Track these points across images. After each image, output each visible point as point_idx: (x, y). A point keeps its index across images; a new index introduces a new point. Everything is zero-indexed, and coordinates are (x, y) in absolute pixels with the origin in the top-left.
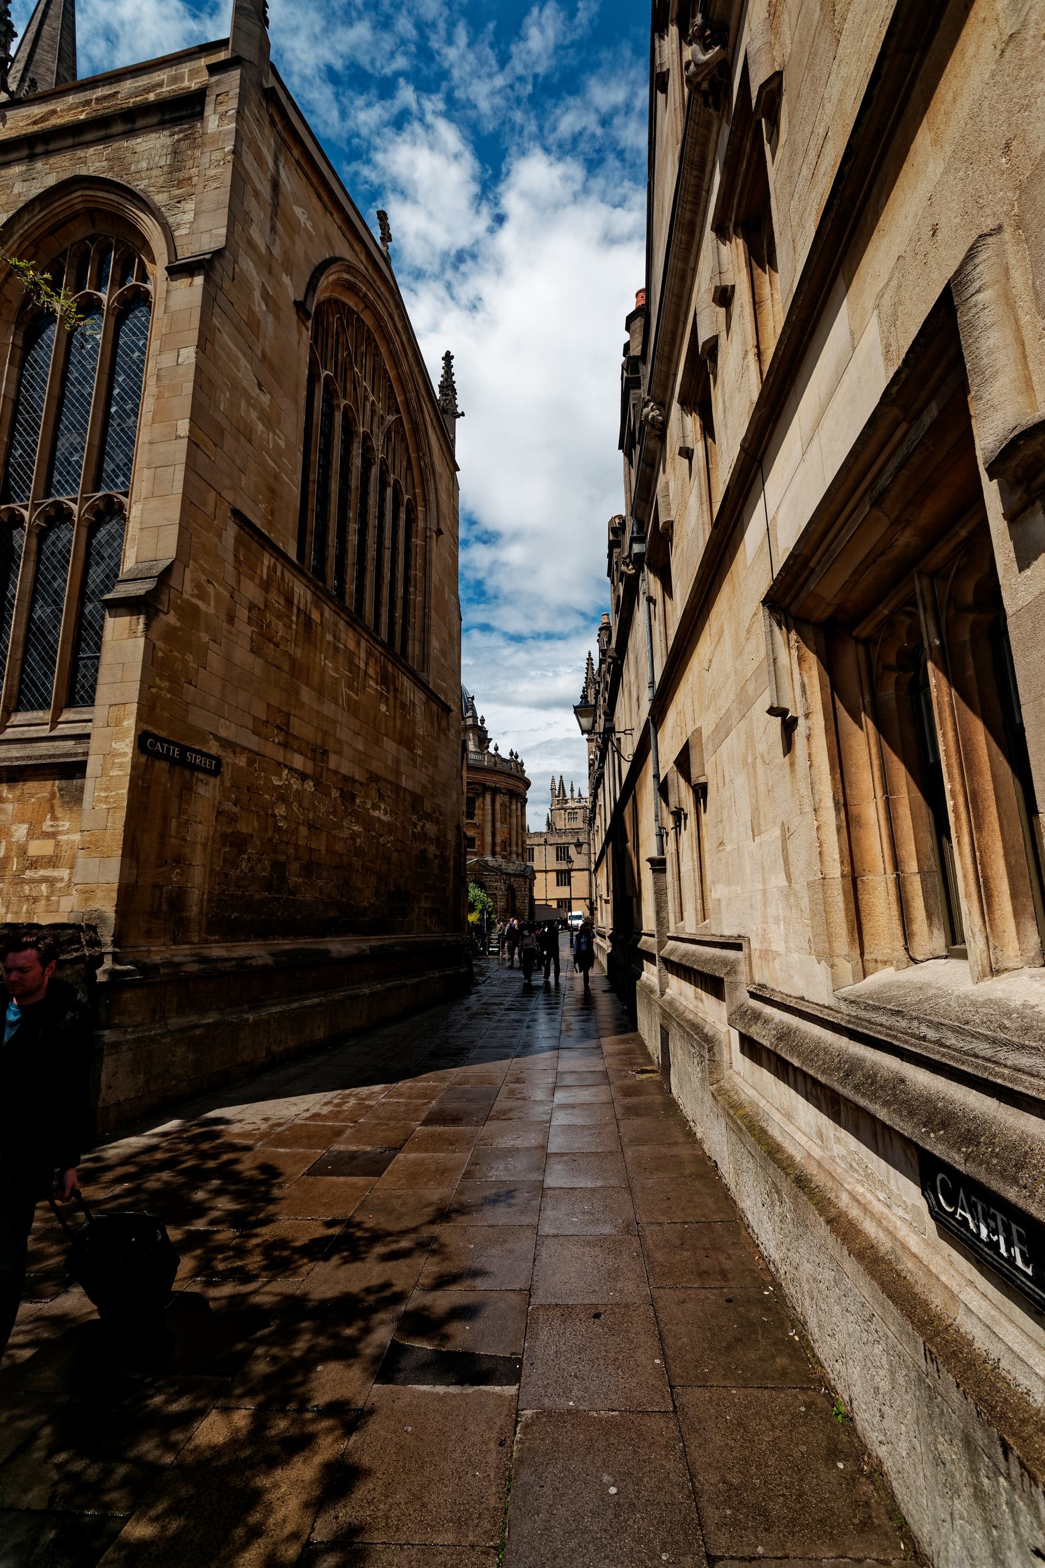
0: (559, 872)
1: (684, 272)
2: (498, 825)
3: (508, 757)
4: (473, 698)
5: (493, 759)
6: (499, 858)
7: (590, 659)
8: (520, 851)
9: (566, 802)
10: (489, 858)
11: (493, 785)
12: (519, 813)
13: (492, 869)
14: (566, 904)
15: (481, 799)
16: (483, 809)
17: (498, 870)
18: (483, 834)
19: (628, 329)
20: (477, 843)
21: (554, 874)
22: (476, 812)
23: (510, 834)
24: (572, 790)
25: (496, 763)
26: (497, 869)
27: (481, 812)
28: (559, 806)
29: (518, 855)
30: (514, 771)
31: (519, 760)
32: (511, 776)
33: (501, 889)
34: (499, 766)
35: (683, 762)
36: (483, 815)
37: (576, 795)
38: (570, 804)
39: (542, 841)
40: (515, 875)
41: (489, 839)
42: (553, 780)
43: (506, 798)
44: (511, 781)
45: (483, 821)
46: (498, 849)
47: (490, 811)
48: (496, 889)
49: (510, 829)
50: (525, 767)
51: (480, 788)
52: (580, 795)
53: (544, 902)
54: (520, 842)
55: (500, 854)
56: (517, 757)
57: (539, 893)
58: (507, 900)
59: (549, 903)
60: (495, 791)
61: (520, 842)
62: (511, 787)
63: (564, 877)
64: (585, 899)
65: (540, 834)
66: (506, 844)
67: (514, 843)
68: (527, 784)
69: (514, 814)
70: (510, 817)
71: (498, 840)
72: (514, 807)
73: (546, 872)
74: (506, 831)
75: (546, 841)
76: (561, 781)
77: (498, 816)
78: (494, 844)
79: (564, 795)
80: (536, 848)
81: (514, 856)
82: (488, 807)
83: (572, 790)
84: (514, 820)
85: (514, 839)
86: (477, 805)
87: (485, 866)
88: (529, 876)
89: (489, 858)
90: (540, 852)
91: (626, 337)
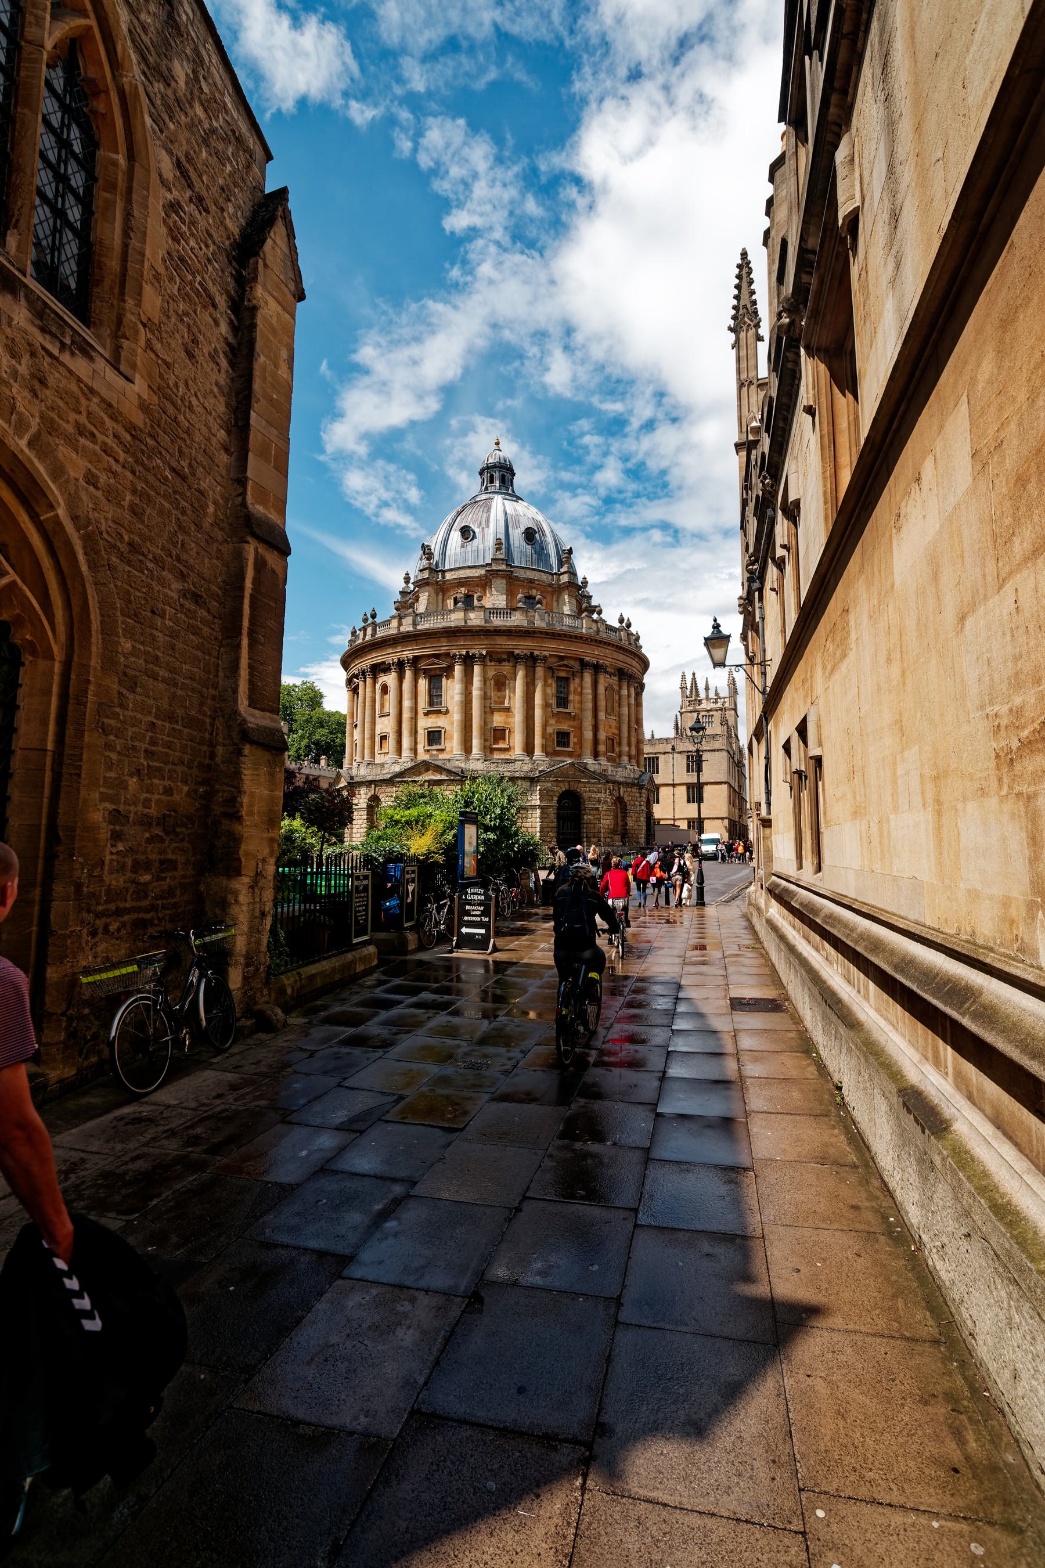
0: (689, 786)
1: (784, 430)
2: (602, 715)
3: (617, 625)
4: (570, 551)
5: (594, 626)
6: (603, 760)
7: (744, 266)
8: (634, 752)
9: (700, 702)
10: (589, 760)
11: (595, 661)
12: (632, 701)
13: (593, 775)
14: (698, 824)
15: (577, 680)
16: (581, 694)
17: (601, 777)
18: (580, 728)
19: (771, 179)
20: (573, 739)
21: (684, 788)
22: (571, 697)
23: (619, 729)
24: (707, 689)
25: (598, 631)
26: (600, 774)
27: (577, 698)
28: (691, 708)
29: (630, 757)
30: (625, 643)
31: (633, 630)
32: (619, 648)
33: (605, 802)
34: (603, 635)
35: (802, 730)
36: (581, 702)
37: (712, 694)
38: (704, 705)
39: (669, 749)
40: (627, 784)
41: (588, 735)
42: (683, 677)
43: (614, 680)
44: (621, 657)
45: (581, 710)
46: (602, 748)
47: (590, 697)
48: (599, 801)
49: (620, 722)
50: (641, 642)
51: (577, 666)
52: (717, 694)
53: (672, 822)
54: (634, 740)
55: (605, 754)
56: (629, 625)
57: (660, 812)
58: (616, 817)
59: (677, 823)
60: (597, 669)
61: (634, 740)
62: (621, 665)
63: (696, 793)
64: (722, 819)
65: (667, 740)
66: (613, 742)
67: (625, 741)
68: (645, 664)
69: (625, 702)
70: (620, 706)
71: (602, 735)
72: (625, 692)
73: (674, 785)
74: (614, 724)
75: (673, 749)
76: (694, 680)
77: (602, 703)
78: (596, 741)
79: (697, 694)
80: (662, 758)
81: (625, 759)
82: (588, 690)
83: (707, 689)
84: (625, 710)
85: (625, 734)
86: (572, 689)
87: (584, 769)
88: (652, 793)
89: (589, 760)
90: (666, 762)
91: (769, 190)
